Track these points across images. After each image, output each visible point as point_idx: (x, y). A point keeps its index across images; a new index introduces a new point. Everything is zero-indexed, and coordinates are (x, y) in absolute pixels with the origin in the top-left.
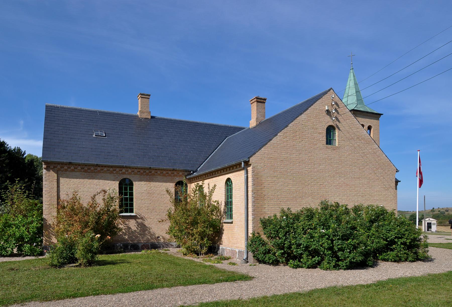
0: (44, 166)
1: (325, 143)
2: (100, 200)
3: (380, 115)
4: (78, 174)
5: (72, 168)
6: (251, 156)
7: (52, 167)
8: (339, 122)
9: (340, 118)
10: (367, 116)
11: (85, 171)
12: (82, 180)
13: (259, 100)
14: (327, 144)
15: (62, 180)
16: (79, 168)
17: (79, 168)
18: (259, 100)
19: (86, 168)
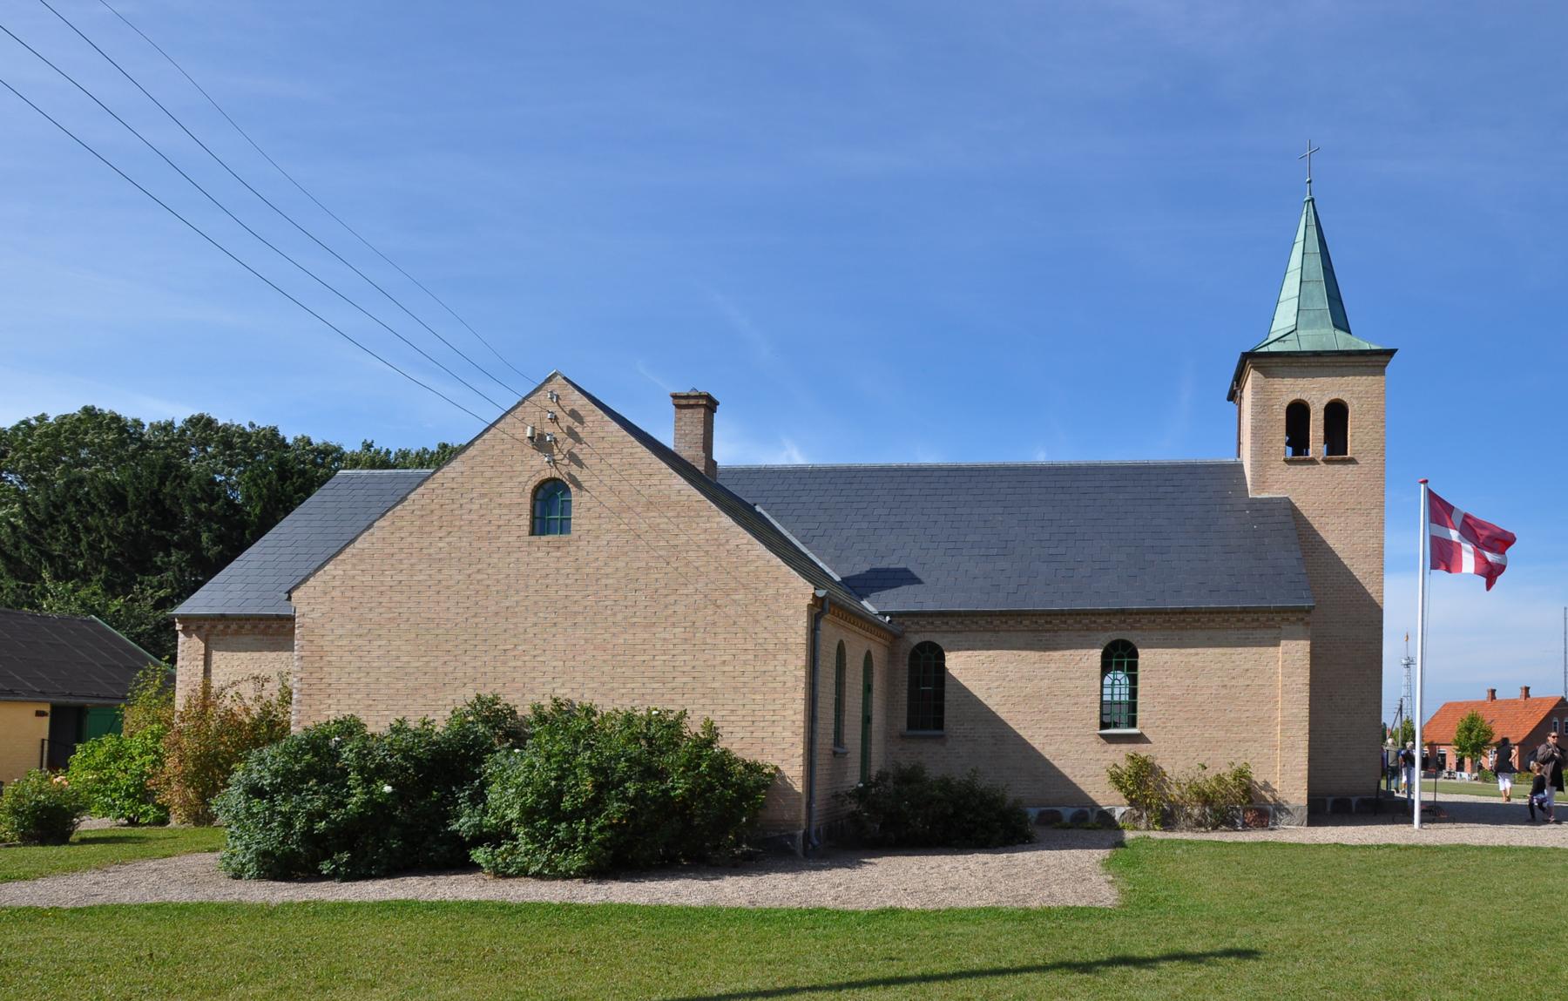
0: (179, 627)
1: (527, 529)
2: (248, 690)
3: (1390, 353)
4: (247, 639)
5: (234, 626)
6: (296, 587)
7: (193, 627)
8: (580, 464)
9: (581, 451)
10: (1322, 365)
11: (264, 633)
12: (256, 655)
13: (684, 402)
14: (532, 533)
15: (216, 656)
16: (248, 626)
17: (248, 626)
18: (684, 402)
19: (262, 626)
